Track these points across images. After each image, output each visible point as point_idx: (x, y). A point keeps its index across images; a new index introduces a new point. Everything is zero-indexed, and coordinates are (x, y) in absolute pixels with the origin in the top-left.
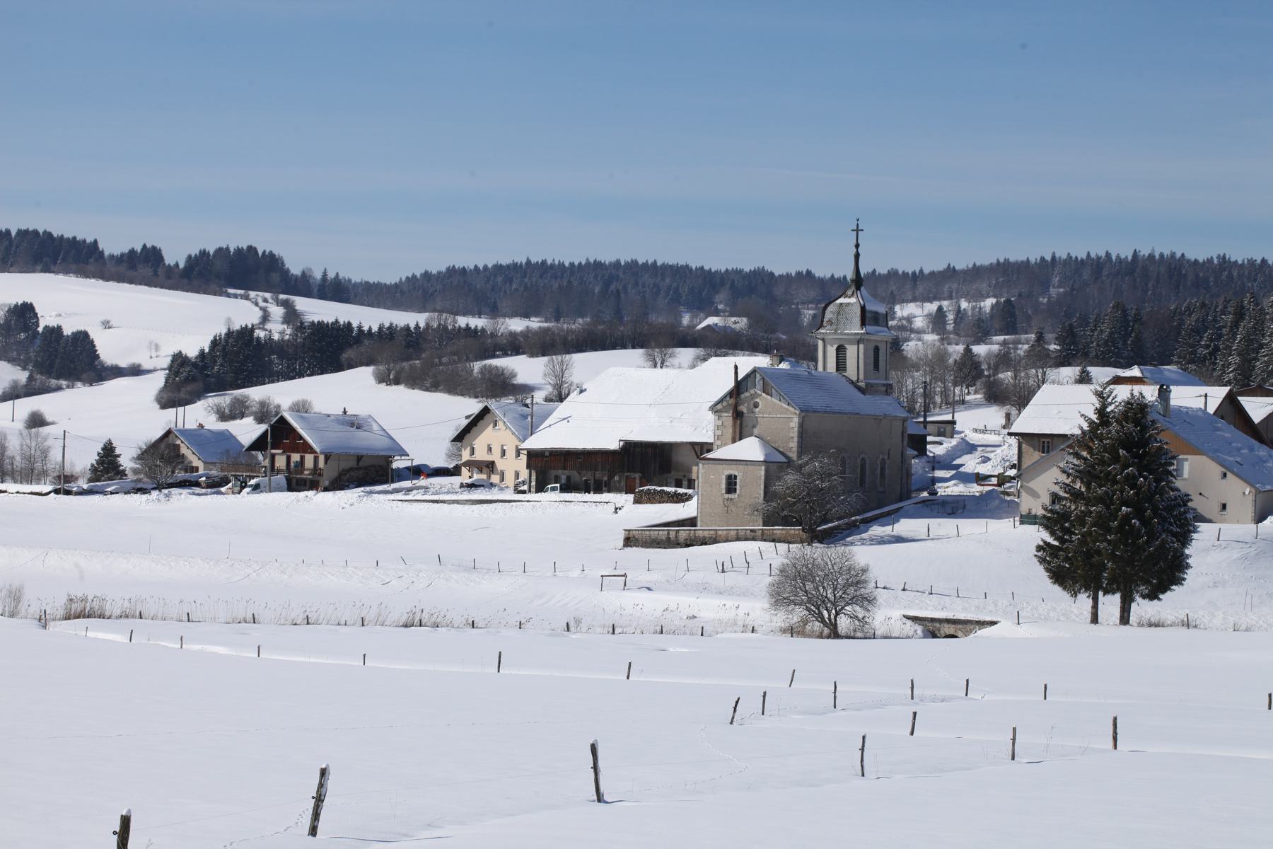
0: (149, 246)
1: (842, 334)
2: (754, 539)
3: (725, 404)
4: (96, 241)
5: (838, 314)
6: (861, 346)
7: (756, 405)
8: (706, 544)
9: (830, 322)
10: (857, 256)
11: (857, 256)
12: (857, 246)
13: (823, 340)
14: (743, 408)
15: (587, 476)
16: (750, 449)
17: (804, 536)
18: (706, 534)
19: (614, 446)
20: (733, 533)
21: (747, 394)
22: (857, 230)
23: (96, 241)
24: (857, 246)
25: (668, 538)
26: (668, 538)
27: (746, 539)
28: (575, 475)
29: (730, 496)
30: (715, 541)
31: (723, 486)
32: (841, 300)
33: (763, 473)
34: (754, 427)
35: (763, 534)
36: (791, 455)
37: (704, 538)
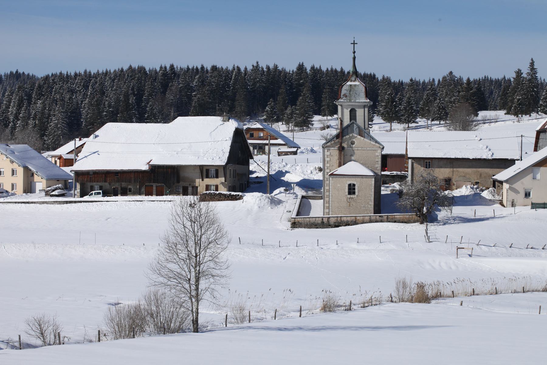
0: (280, 68)
1: (355, 102)
2: (382, 221)
3: (333, 142)
4: (342, 69)
5: (350, 91)
6: (366, 109)
7: (353, 143)
8: (349, 225)
9: (345, 96)
10: (354, 58)
11: (354, 58)
12: (354, 52)
13: (341, 105)
14: (345, 145)
15: (117, 185)
16: (353, 168)
17: (416, 218)
18: (349, 219)
19: (145, 168)
20: (367, 218)
21: (347, 137)
22: (354, 44)
23: (342, 69)
24: (354, 52)
25: (323, 222)
26: (323, 222)
27: (377, 222)
28: (106, 185)
29: (351, 196)
30: (355, 223)
31: (347, 190)
32: (349, 83)
33: (373, 182)
34: (352, 155)
35: (387, 218)
36: (376, 171)
37: (348, 221)
